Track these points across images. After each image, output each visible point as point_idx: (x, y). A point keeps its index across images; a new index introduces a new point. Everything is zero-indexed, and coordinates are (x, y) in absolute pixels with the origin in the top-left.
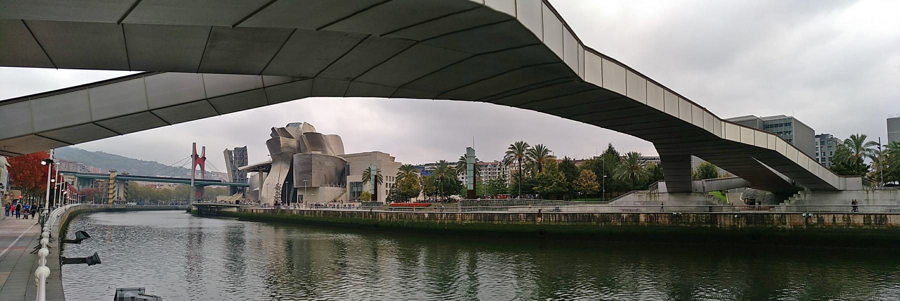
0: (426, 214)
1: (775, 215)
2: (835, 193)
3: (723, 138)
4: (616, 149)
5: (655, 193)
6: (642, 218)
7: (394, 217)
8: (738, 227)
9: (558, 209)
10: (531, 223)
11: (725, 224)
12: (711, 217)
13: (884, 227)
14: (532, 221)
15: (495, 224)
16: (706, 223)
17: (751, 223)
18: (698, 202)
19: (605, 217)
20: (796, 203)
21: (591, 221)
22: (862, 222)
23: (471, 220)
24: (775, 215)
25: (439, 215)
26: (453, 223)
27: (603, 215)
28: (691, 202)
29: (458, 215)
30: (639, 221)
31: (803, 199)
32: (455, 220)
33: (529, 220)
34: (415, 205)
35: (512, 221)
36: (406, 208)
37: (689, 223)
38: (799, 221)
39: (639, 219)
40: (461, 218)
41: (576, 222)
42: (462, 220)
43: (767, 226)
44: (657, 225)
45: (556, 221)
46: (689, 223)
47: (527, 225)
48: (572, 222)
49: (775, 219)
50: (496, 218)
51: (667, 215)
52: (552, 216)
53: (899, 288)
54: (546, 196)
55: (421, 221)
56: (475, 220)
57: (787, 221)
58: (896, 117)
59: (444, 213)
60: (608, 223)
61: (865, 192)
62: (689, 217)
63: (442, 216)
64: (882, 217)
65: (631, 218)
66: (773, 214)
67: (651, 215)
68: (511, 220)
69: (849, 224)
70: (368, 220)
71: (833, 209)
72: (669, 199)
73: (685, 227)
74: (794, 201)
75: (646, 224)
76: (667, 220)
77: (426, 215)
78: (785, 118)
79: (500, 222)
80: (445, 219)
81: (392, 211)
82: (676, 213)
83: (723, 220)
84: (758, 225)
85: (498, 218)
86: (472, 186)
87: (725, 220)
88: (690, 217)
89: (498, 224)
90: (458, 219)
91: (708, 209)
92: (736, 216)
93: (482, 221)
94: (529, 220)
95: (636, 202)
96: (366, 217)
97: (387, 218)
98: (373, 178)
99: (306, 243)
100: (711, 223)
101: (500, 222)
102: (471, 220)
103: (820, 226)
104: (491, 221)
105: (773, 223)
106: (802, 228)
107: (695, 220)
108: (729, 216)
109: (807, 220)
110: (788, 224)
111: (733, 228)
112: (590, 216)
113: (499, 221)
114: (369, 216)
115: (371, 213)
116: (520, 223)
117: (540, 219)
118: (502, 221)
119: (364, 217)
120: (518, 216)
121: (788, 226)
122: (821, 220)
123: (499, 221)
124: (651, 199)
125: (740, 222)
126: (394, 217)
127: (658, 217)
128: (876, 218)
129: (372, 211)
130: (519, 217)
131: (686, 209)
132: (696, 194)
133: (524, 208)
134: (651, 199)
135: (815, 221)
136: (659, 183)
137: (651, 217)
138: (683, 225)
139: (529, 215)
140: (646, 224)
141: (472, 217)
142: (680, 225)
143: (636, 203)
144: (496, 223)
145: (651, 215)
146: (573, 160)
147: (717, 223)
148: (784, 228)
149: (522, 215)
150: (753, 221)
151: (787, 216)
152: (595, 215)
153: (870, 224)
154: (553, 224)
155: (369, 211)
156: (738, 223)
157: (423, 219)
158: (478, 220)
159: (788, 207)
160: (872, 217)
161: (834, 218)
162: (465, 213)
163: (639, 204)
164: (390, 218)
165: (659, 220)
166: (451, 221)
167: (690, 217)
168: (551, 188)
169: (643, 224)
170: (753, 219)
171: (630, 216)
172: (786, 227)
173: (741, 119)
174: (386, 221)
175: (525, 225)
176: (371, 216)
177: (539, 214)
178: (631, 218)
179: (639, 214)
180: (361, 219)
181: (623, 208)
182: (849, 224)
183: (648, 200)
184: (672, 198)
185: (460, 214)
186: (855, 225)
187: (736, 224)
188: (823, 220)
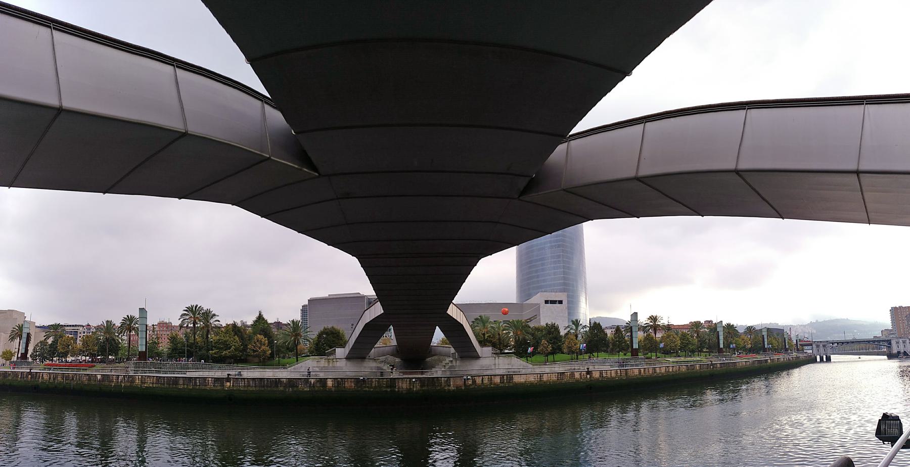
0: (98, 376)
1: (443, 379)
2: (476, 359)
3: (875, 432)
4: (265, 317)
5: (333, 359)
6: (330, 383)
7: (59, 379)
8: (414, 390)
9: (240, 374)
10: (219, 388)
11: (402, 388)
12: (391, 382)
13: (511, 385)
14: (220, 386)
15: (180, 389)
16: (387, 387)
17: (425, 386)
18: (371, 368)
19: (291, 382)
20: (449, 368)
21: (278, 386)
22: (499, 381)
23: (153, 383)
24: (443, 379)
25: (114, 377)
26: (131, 386)
27: (290, 380)
28: (365, 367)
29: (137, 377)
30: (326, 386)
31: (455, 365)
32: (133, 383)
33: (216, 385)
34: (83, 366)
35: (200, 385)
36: (69, 369)
37: (372, 388)
38: (460, 382)
39: (326, 384)
40: (141, 380)
41: (264, 387)
42: (142, 382)
43: (437, 388)
44: (343, 389)
45: (244, 386)
46: (372, 388)
47: (215, 390)
48: (259, 387)
49: (443, 382)
50: (181, 382)
51: (353, 380)
52: (242, 381)
53: (637, 462)
54: (220, 360)
55: (93, 383)
56: (158, 384)
57: (451, 383)
58: (460, 303)
59: (121, 375)
60: (295, 389)
61: (494, 358)
62: (372, 382)
63: (118, 378)
64: (510, 377)
65: (318, 383)
66: (441, 377)
67: (339, 379)
68: (198, 384)
69: (491, 383)
70: (25, 381)
71: (474, 373)
72: (346, 363)
73: (369, 391)
74: (448, 367)
75: (333, 389)
76: (353, 385)
77: (99, 377)
78: (359, 295)
79: (186, 386)
80: (121, 382)
81: (51, 372)
82: (362, 378)
83: (400, 384)
84: (430, 387)
85: (184, 383)
86: (144, 347)
87: (402, 384)
88: (373, 382)
89: (184, 388)
90: (137, 381)
91: (379, 374)
92: (414, 380)
93: (166, 385)
94: (216, 385)
95: (314, 367)
96: (24, 378)
97: (50, 378)
98: (24, 336)
99: (430, 461)
100: (391, 387)
101: (186, 386)
102: (153, 383)
103: (473, 386)
104: (176, 385)
105: (441, 385)
106: (462, 389)
107: (377, 385)
108: (406, 380)
109: (465, 382)
110: (452, 386)
111: (409, 391)
112: (277, 382)
113: (184, 385)
114: (27, 376)
115: (30, 373)
116: (208, 388)
117: (228, 384)
118: (187, 385)
119: (21, 378)
120: (206, 380)
121: (452, 388)
122: (474, 382)
123: (184, 385)
124: (329, 365)
125: (415, 385)
126: (59, 379)
127: (345, 382)
128: (507, 378)
129: (32, 371)
130: (207, 381)
131: (359, 374)
132: (370, 360)
133: (205, 372)
134: (329, 365)
135: (470, 382)
136: (336, 349)
137: (339, 382)
138: (367, 389)
139: (217, 380)
140: (333, 389)
141: (155, 380)
142: (365, 389)
143: (314, 369)
144: (182, 387)
145: (339, 379)
146: (225, 325)
147: (396, 387)
148: (449, 389)
149: (210, 379)
150: (426, 384)
151: (451, 379)
152: (282, 380)
153: (503, 382)
154: (242, 389)
155: (29, 371)
156: (413, 386)
157: (95, 381)
158: (161, 384)
159: (444, 372)
160: (505, 377)
161: (483, 379)
162: (145, 376)
163: (317, 369)
164: (54, 379)
165: (346, 385)
166: (128, 384)
167: (373, 382)
168: (229, 352)
169: (330, 390)
170: (426, 382)
171: (318, 381)
172: (450, 388)
173: (338, 296)
174: (49, 382)
175: (213, 389)
176: (30, 376)
177: (228, 379)
178: (318, 383)
179: (327, 379)
180: (17, 380)
181: (302, 373)
182: (491, 383)
183: (326, 365)
184: (349, 363)
185: (140, 377)
186: (495, 384)
187: (412, 387)
188: (475, 381)
